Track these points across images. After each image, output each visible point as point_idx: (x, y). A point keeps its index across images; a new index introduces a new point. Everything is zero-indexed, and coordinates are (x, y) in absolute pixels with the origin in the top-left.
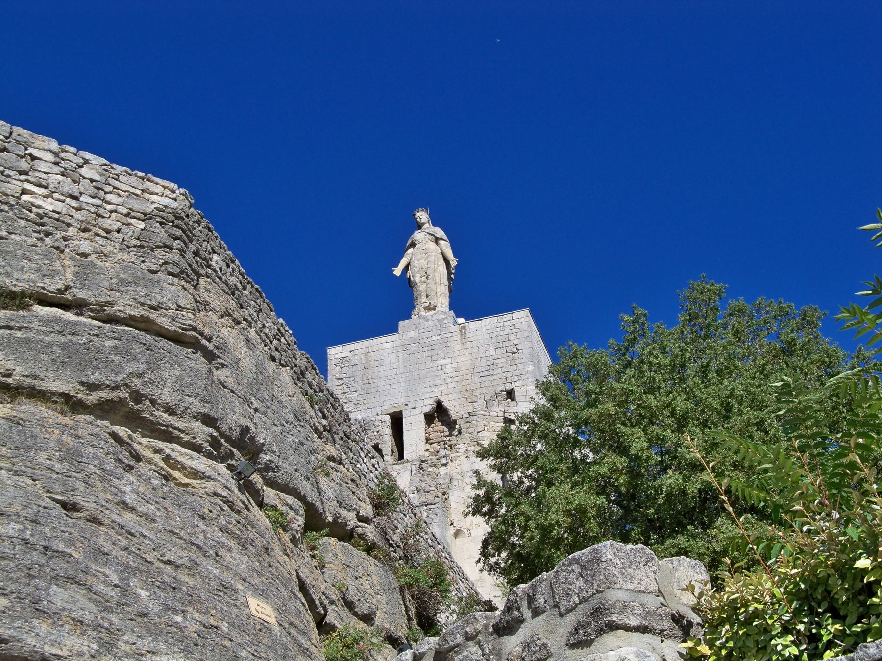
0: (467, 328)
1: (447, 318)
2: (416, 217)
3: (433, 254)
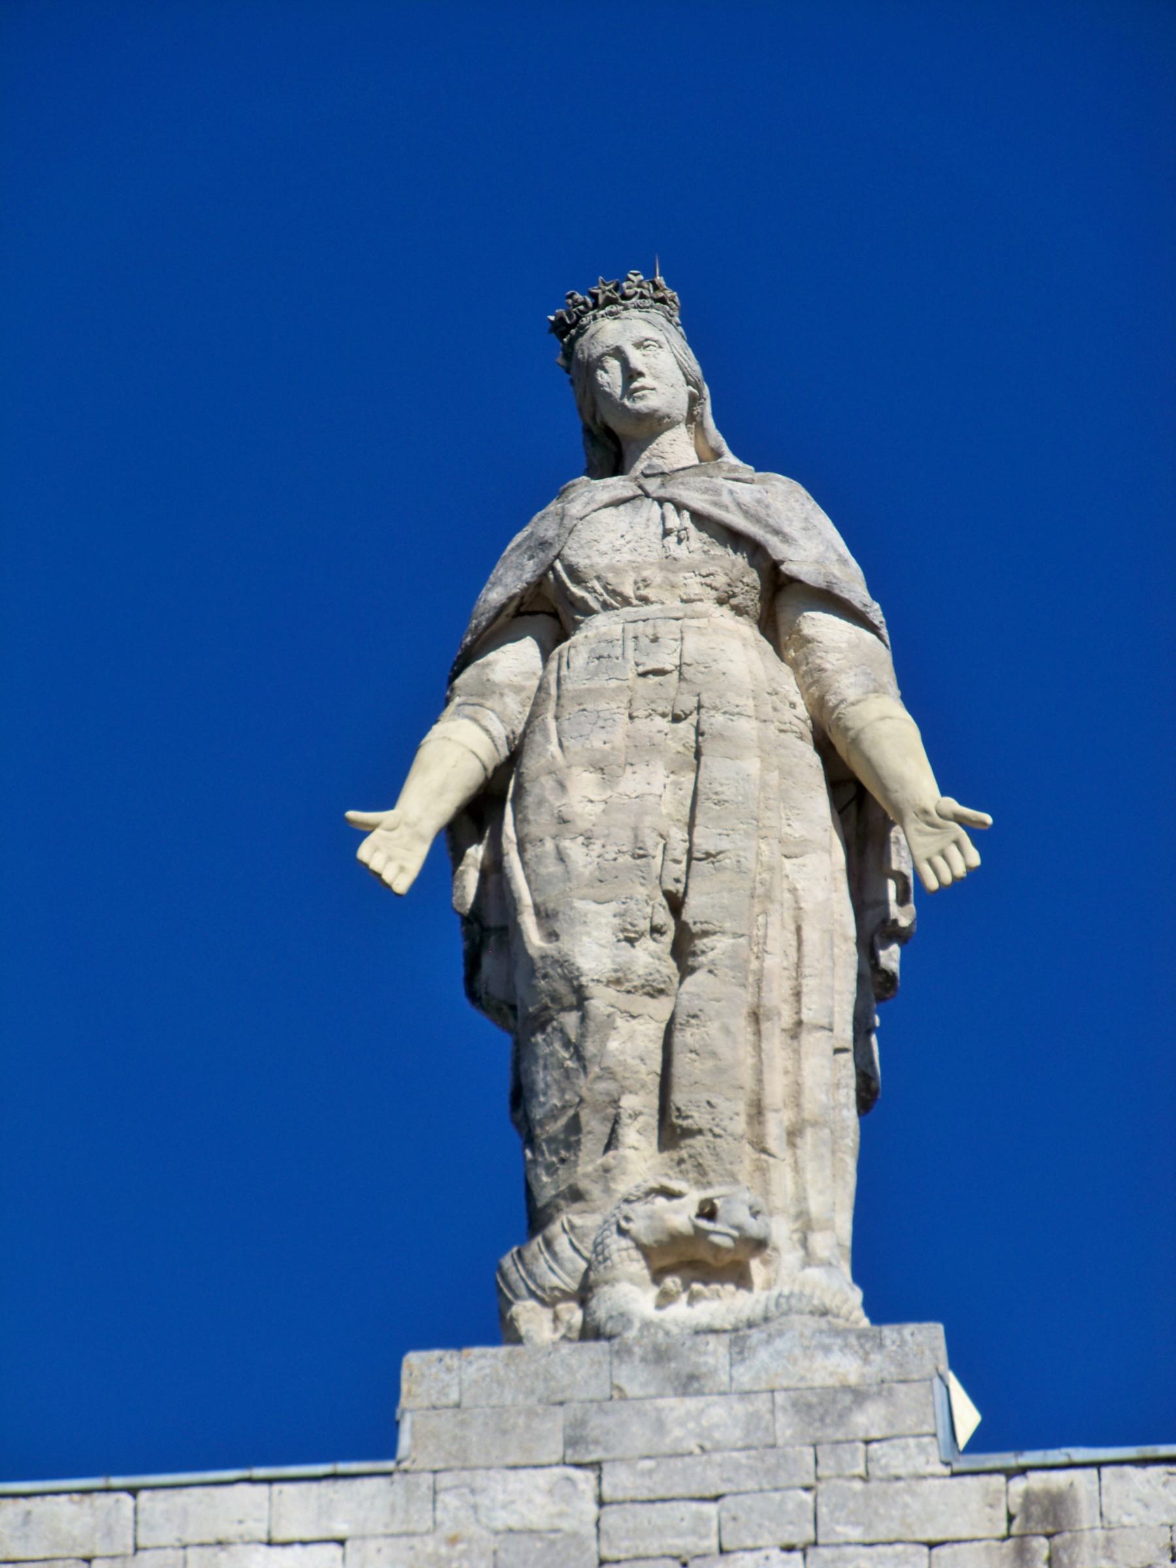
0: (1086, 1516)
1: (881, 1389)
2: (588, 347)
3: (747, 727)
